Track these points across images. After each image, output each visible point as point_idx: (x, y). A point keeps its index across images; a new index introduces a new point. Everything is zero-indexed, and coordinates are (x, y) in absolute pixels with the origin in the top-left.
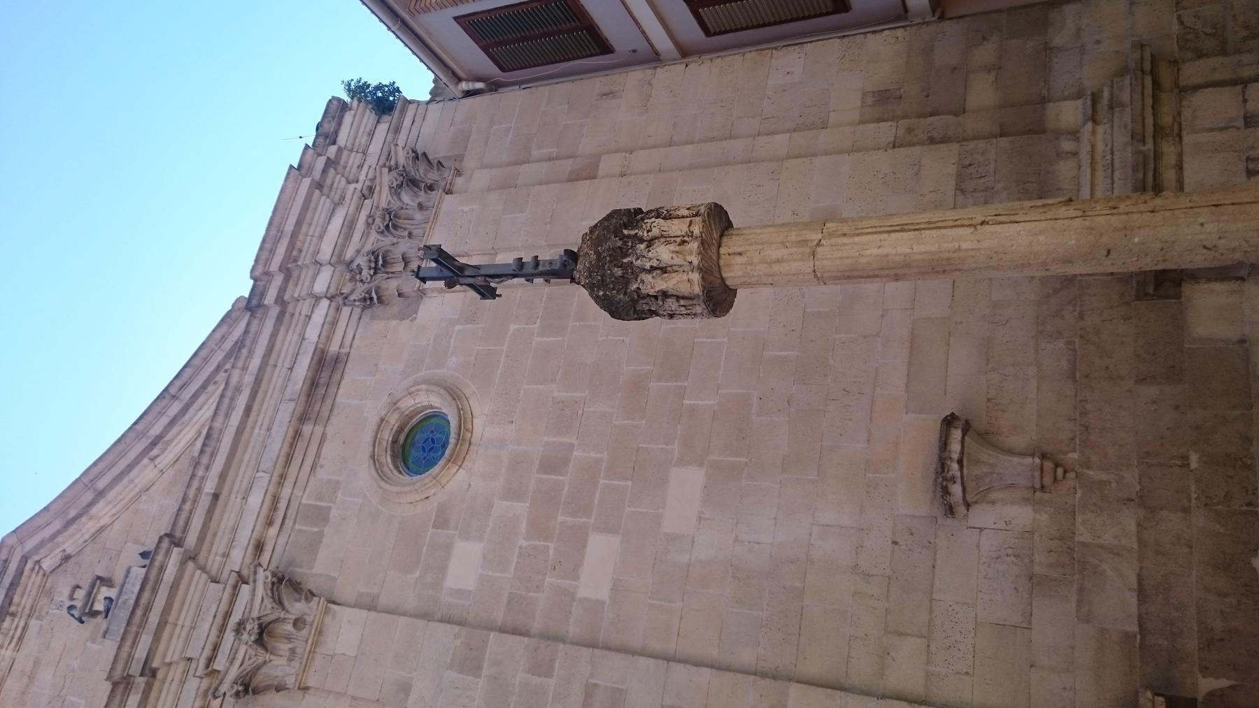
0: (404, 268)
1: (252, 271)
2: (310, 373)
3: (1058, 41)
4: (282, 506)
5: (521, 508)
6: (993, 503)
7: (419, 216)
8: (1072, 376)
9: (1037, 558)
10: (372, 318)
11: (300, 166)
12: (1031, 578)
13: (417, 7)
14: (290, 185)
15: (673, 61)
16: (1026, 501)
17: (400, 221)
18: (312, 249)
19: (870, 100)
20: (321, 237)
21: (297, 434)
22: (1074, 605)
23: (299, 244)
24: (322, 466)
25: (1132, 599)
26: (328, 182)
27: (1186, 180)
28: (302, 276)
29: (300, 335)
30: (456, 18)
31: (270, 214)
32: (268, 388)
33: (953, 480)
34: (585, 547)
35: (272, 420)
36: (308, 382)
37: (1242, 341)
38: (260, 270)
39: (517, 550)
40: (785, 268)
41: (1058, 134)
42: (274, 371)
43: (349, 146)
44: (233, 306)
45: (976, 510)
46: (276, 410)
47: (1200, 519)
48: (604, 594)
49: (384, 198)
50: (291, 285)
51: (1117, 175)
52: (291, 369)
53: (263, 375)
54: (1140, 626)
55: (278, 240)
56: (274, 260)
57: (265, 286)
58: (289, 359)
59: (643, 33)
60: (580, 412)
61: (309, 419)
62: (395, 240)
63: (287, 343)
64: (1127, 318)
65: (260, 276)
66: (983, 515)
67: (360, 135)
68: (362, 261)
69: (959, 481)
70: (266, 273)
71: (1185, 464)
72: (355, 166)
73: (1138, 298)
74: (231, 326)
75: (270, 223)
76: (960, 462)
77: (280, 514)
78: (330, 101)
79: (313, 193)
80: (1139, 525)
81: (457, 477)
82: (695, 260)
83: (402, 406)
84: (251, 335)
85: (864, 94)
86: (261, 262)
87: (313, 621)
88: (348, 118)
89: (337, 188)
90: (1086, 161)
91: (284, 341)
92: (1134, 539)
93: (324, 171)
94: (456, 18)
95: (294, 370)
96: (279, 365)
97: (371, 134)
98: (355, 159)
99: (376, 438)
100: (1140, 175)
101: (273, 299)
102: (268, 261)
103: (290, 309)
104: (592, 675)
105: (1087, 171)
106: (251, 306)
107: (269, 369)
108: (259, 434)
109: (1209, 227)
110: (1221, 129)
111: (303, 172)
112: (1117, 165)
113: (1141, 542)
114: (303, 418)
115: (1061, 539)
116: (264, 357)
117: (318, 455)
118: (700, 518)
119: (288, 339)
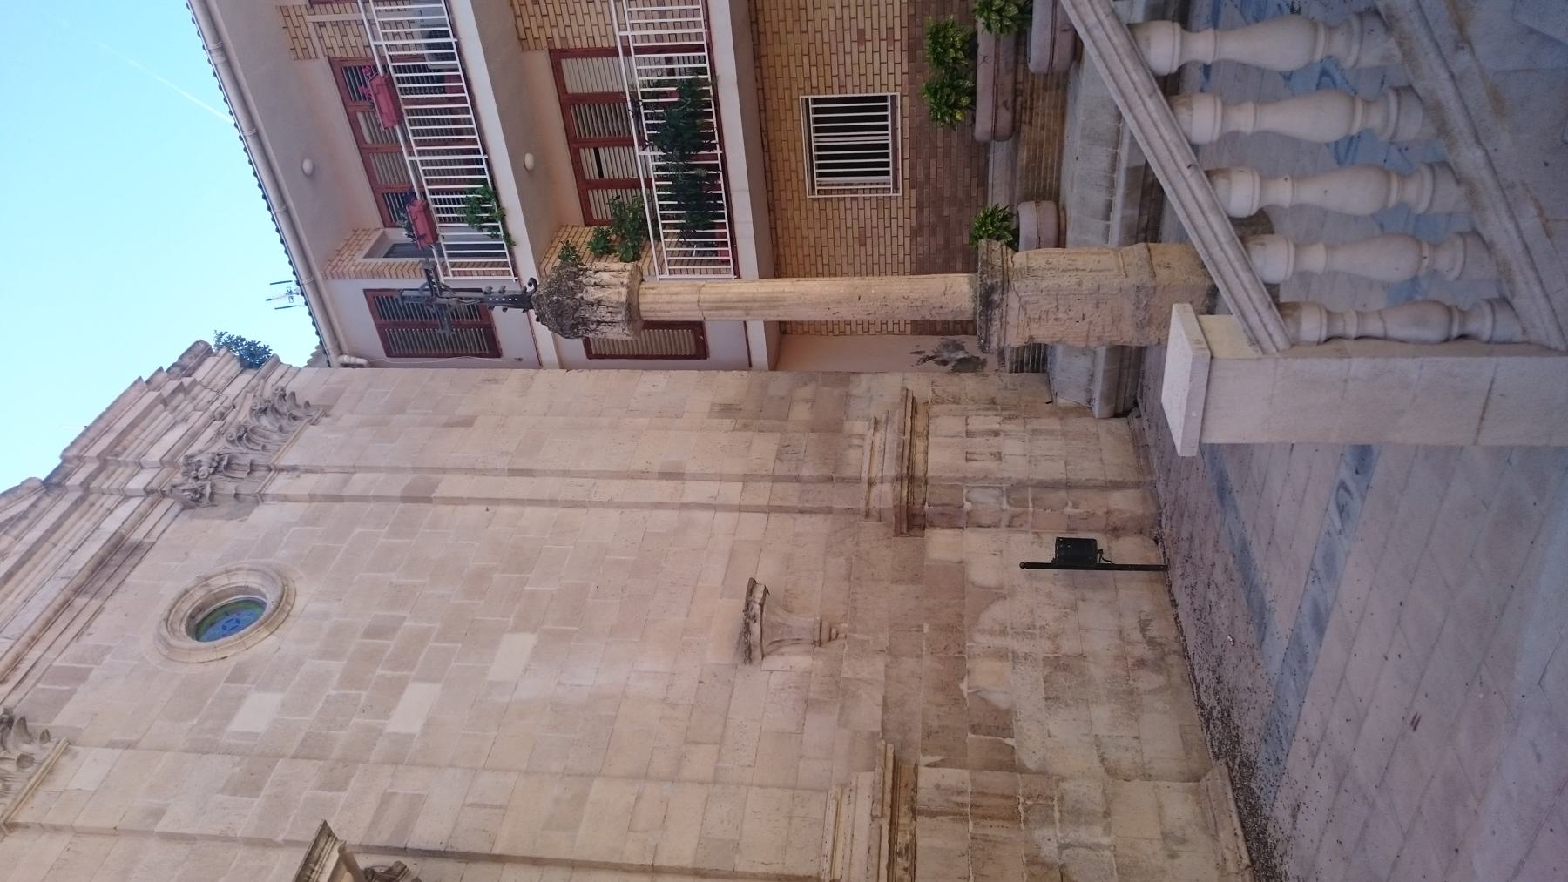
0: (249, 474)
1: (66, 450)
2: (101, 552)
3: (854, 392)
4: (24, 667)
5: (336, 667)
6: (783, 654)
7: (275, 437)
8: (848, 578)
9: (812, 688)
10: (192, 517)
11: (148, 382)
12: (806, 701)
13: (334, 271)
14: (133, 393)
15: (552, 367)
16: (808, 653)
17: (255, 437)
18: (139, 450)
19: (717, 409)
20: (152, 444)
21: (67, 604)
22: (836, 717)
23: (125, 442)
24: (90, 634)
25: (878, 711)
26: (174, 403)
27: (930, 461)
28: (118, 472)
29: (95, 524)
30: (366, 291)
31: (103, 409)
32: (39, 563)
33: (754, 618)
34: (402, 693)
35: (33, 594)
36: (96, 560)
37: (961, 562)
38: (74, 452)
39: (324, 698)
40: (680, 298)
41: (851, 436)
42: (51, 550)
43: (205, 382)
44: (23, 483)
45: (767, 659)
46: (41, 585)
47: (928, 661)
48: (416, 728)
49: (243, 416)
50: (102, 476)
51: (886, 456)
52: (73, 552)
53: (39, 549)
54: (882, 726)
55: (104, 433)
56: (94, 448)
57: (72, 469)
58: (74, 541)
59: (534, 340)
60: (418, 594)
61: (86, 593)
62: (245, 451)
63: (76, 528)
64: (887, 547)
65: (71, 459)
66: (774, 662)
67: (220, 376)
68: (205, 458)
69: (759, 620)
70: (80, 458)
71: (920, 629)
72: (206, 400)
73: (896, 535)
74: (11, 502)
75: (101, 417)
76: (762, 605)
77: (19, 674)
78: (197, 342)
79: (156, 406)
80: (886, 666)
81: (265, 642)
82: (626, 281)
83: (213, 584)
84: (38, 510)
85: (713, 404)
86: (79, 446)
87: (44, 760)
88: (210, 362)
89: (182, 411)
90: (867, 447)
91: (73, 525)
92: (883, 674)
93: (174, 392)
94: (366, 291)
95: (76, 553)
96: (60, 545)
97: (231, 381)
98: (208, 395)
99: (174, 606)
100: (901, 450)
101: (79, 482)
102: (86, 447)
103: (92, 498)
104: (391, 786)
105: (868, 454)
106: (52, 485)
107: (47, 546)
108: (11, 603)
109: (906, 287)
110: (953, 437)
111: (152, 387)
112: (887, 450)
113: (886, 676)
114: (78, 591)
115: (831, 675)
116: (47, 531)
117: (88, 624)
118: (526, 670)
119: (79, 526)
